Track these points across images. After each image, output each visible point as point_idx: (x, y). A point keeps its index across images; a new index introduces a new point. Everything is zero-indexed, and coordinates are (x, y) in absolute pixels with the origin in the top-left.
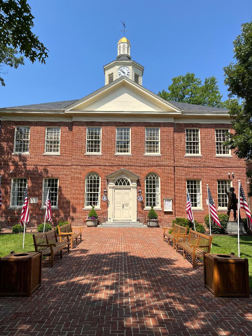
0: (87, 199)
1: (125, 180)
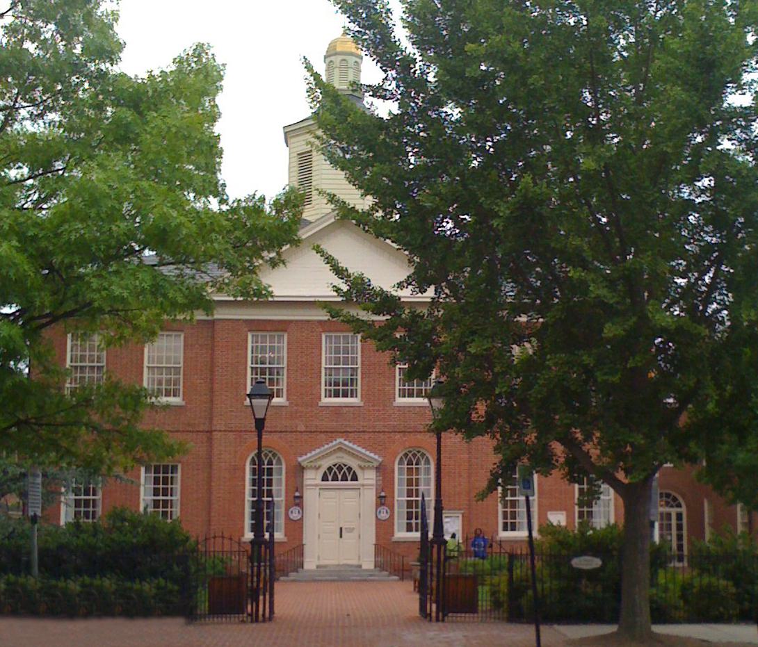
0: (174, 504)
1: (345, 469)
